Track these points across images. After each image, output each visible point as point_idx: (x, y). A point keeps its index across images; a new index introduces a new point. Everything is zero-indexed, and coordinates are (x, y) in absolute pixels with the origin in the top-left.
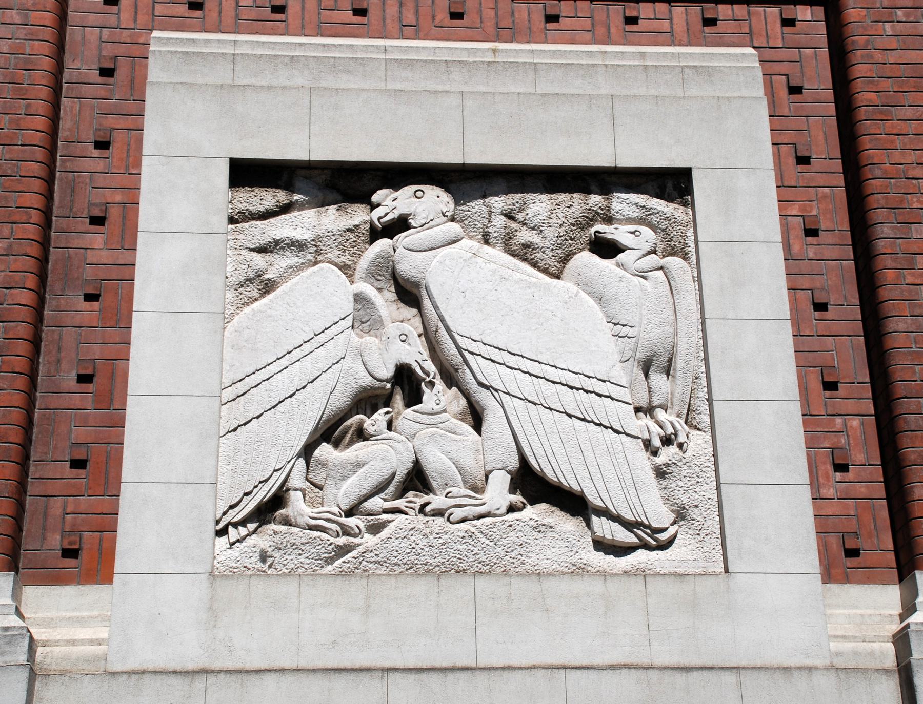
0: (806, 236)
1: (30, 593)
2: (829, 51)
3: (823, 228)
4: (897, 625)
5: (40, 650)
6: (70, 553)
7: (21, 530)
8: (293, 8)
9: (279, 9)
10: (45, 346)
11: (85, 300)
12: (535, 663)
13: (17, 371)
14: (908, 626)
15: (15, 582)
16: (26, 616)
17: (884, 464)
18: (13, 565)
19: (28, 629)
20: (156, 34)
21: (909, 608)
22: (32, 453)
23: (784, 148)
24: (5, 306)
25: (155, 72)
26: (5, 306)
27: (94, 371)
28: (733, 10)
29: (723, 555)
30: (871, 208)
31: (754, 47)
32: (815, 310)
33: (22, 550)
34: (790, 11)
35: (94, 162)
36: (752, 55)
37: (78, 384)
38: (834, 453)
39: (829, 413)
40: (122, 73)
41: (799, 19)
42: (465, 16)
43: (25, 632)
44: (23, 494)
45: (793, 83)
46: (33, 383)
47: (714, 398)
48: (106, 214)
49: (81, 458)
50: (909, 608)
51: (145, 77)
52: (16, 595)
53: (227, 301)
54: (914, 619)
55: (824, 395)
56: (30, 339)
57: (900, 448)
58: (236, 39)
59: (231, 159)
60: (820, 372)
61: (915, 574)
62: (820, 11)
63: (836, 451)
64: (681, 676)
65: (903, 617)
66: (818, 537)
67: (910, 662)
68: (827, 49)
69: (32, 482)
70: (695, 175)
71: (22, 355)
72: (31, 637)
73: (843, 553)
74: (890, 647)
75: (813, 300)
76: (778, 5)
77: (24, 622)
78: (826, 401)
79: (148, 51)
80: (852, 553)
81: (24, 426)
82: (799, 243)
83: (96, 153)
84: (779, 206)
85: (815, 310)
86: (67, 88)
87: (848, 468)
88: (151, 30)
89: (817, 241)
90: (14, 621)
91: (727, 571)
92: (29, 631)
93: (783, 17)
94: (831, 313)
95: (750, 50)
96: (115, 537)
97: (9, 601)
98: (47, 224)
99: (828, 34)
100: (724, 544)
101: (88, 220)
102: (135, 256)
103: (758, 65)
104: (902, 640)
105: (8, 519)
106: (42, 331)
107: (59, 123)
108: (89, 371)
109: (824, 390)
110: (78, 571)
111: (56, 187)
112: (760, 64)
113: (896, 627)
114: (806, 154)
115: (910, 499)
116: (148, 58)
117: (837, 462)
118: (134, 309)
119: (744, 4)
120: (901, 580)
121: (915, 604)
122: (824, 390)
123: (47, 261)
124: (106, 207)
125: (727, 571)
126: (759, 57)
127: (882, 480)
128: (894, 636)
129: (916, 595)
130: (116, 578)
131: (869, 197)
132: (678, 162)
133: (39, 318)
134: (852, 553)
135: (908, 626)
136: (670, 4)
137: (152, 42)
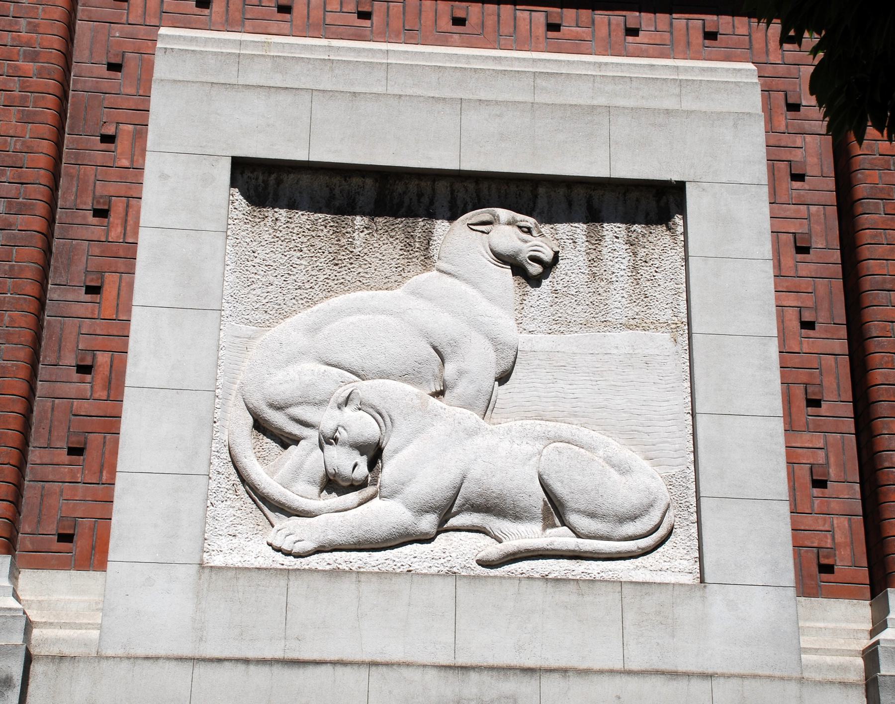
1: (27, 577)
3: (804, 103)
4: (866, 641)
5: (36, 632)
6: (66, 538)
7: (32, 411)
8: (299, 8)
9: (285, 9)
14: (878, 642)
15: (12, 565)
16: (21, 598)
17: (855, 401)
18: (10, 548)
20: (163, 31)
21: (879, 624)
22: (32, 439)
23: (783, 237)
25: (162, 68)
27: (123, 61)
28: (733, 21)
29: (698, 540)
30: (876, 417)
31: (753, 63)
32: (797, 253)
35: (98, 153)
37: (79, 375)
39: (794, 203)
40: (92, 454)
41: (803, 104)
42: (467, 22)
43: (21, 614)
44: (17, 515)
45: (790, 101)
46: (23, 455)
49: (110, 133)
50: (879, 624)
52: (13, 576)
54: (883, 636)
57: (875, 434)
58: (243, 39)
59: (233, 157)
61: (887, 591)
63: (821, 550)
65: (873, 633)
67: (877, 648)
69: (42, 367)
70: (690, 189)
71: (48, 138)
72: (27, 618)
74: (860, 662)
75: (801, 319)
78: (807, 418)
79: (157, 35)
80: (826, 569)
82: (790, 257)
83: (96, 220)
84: (780, 357)
85: (797, 253)
86: (73, 96)
87: (827, 484)
88: (159, 27)
89: (823, 493)
90: (12, 603)
91: (702, 580)
92: (24, 613)
94: (824, 409)
95: (751, 66)
97: (6, 583)
98: (51, 220)
99: (836, 177)
101: (56, 537)
102: (141, 191)
103: (757, 81)
104: (871, 656)
105: (58, 68)
106: (43, 320)
107: (60, 180)
108: (88, 362)
110: (72, 556)
111: (69, 105)
112: (759, 80)
113: (866, 642)
118: (127, 383)
119: (746, 17)
120: (873, 595)
121: (886, 621)
123: (57, 189)
124: (86, 438)
125: (702, 580)
128: (864, 651)
129: (887, 612)
130: (110, 565)
131: (866, 341)
132: (673, 176)
133: (33, 373)
134: (826, 569)
135: (878, 642)
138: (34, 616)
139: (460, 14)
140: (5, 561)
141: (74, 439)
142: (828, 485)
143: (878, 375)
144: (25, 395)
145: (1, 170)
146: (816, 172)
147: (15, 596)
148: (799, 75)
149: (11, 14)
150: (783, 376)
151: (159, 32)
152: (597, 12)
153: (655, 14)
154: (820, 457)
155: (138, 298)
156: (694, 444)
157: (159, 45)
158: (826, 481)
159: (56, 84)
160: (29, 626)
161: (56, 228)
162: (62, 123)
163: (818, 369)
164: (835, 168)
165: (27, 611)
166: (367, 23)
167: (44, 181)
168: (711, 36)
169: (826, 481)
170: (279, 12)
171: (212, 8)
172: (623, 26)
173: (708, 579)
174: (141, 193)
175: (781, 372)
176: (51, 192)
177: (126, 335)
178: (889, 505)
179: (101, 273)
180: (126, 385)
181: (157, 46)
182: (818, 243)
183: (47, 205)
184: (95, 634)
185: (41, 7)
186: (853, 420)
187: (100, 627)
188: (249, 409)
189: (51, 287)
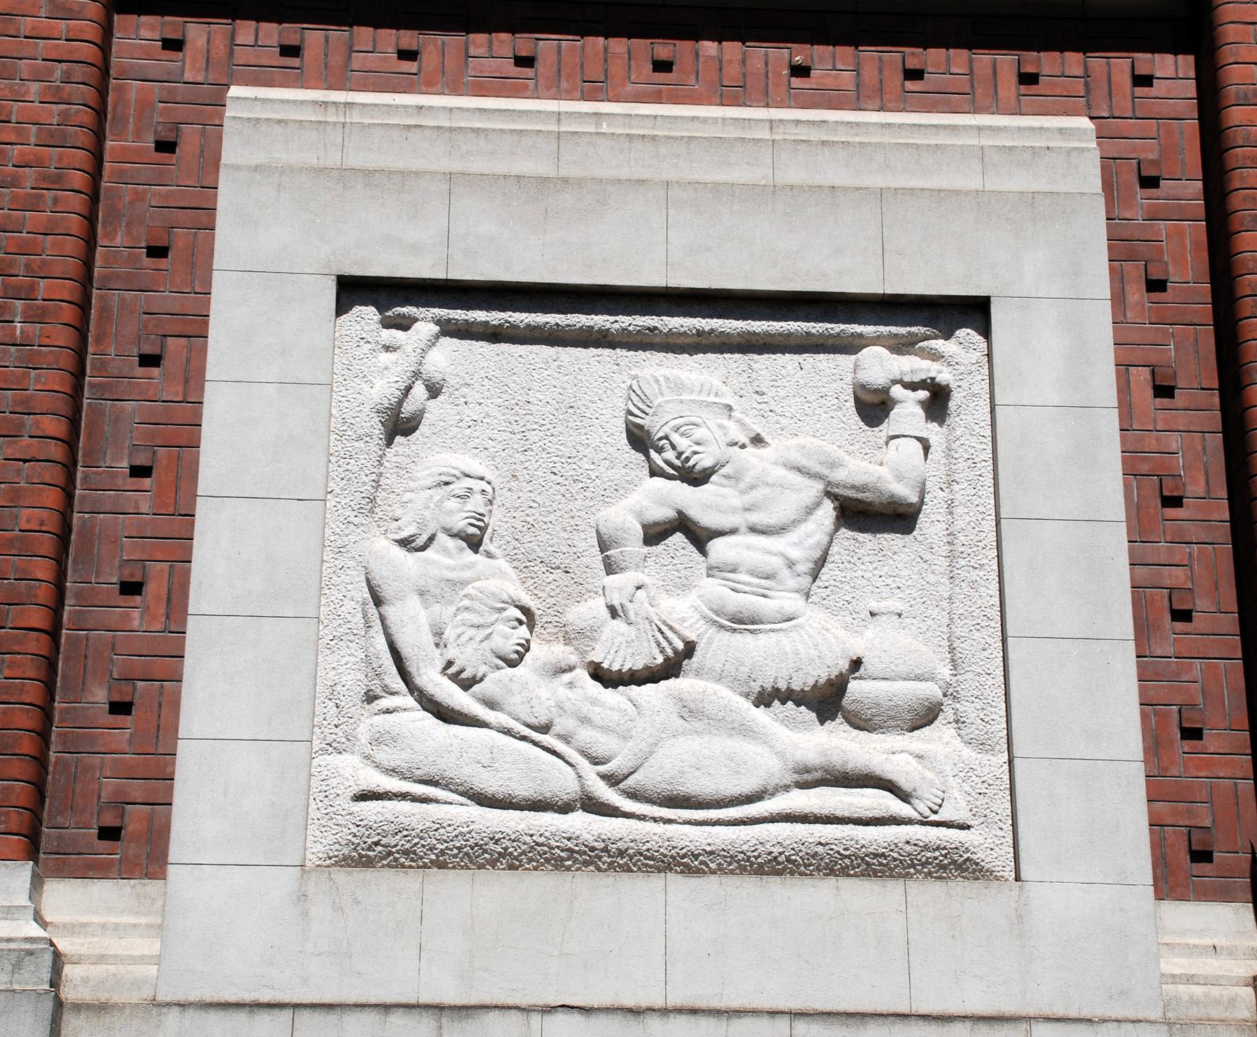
0: (1192, 862)
2: (1212, 287)
5: (68, 970)
6: (110, 834)
10: (106, 258)
11: (148, 256)
12: (739, 1020)
13: (77, 189)
17: (1223, 390)
18: (32, 851)
19: (51, 940)
20: (234, 91)
24: (44, 257)
25: (233, 151)
26: (44, 257)
31: (1091, 118)
33: (111, 78)
34: (1146, 62)
36: (1085, 131)
37: (149, 259)
38: (1183, 711)
41: (1158, 76)
47: (1009, 634)
48: (153, 463)
51: (175, 727)
53: (314, 751)
55: (1173, 629)
56: (56, 532)
60: (1130, 64)
62: (1185, 64)
64: (941, 886)
66: (1151, 832)
68: (1237, 615)
73: (1188, 857)
75: (1154, 382)
76: (1128, 51)
77: (45, 930)
80: (1201, 856)
81: (96, 108)
88: (227, 86)
90: (35, 931)
91: (1017, 879)
92: (52, 944)
93: (1164, 494)
94: (1180, 398)
95: (1084, 123)
96: (205, 345)
100: (1007, 694)
103: (1094, 145)
108: (171, 137)
109: (1155, 397)
111: (92, 311)
112: (1098, 144)
114: (1154, 173)
115: (1243, 385)
116: (225, 106)
117: (1185, 725)
122: (1155, 397)
125: (1017, 879)
126: (1097, 132)
127: (1249, 751)
131: (1226, 154)
136: (857, 48)
137: (228, 103)
138: (63, 945)
139: (912, 64)
140: (23, 872)
141: (126, 572)
142: (1161, 185)
143: (1236, 115)
144: (30, 807)
145: (1, 372)
146: (1200, 490)
147: (39, 919)
148: (1159, 136)
149: (14, 119)
150: (1143, 692)
151: (229, 94)
152: (517, 35)
153: (1176, 55)
154: (1177, 577)
155: (212, 371)
156: (1002, 625)
157: (229, 112)
158: (1201, 729)
159: (96, 27)
160: (58, 960)
161: (97, 255)
162: (74, 457)
163: (1155, 139)
164: (1210, 265)
165: (54, 940)
166: (529, 72)
167: (78, 208)
168: (1028, 79)
169: (1201, 729)
170: (399, 58)
171: (303, 55)
172: (901, 67)
173: (1024, 874)
174: (184, 651)
175: (1121, 436)
176: (77, 332)
177: (205, 314)
178: (1243, 215)
179: (176, 127)
180: (214, 268)
181: (226, 115)
182: (1201, 604)
183: (51, 611)
184: (153, 969)
185: (33, 373)
186: (1229, 524)
187: (157, 960)
188: (368, 581)
189: (57, 758)
